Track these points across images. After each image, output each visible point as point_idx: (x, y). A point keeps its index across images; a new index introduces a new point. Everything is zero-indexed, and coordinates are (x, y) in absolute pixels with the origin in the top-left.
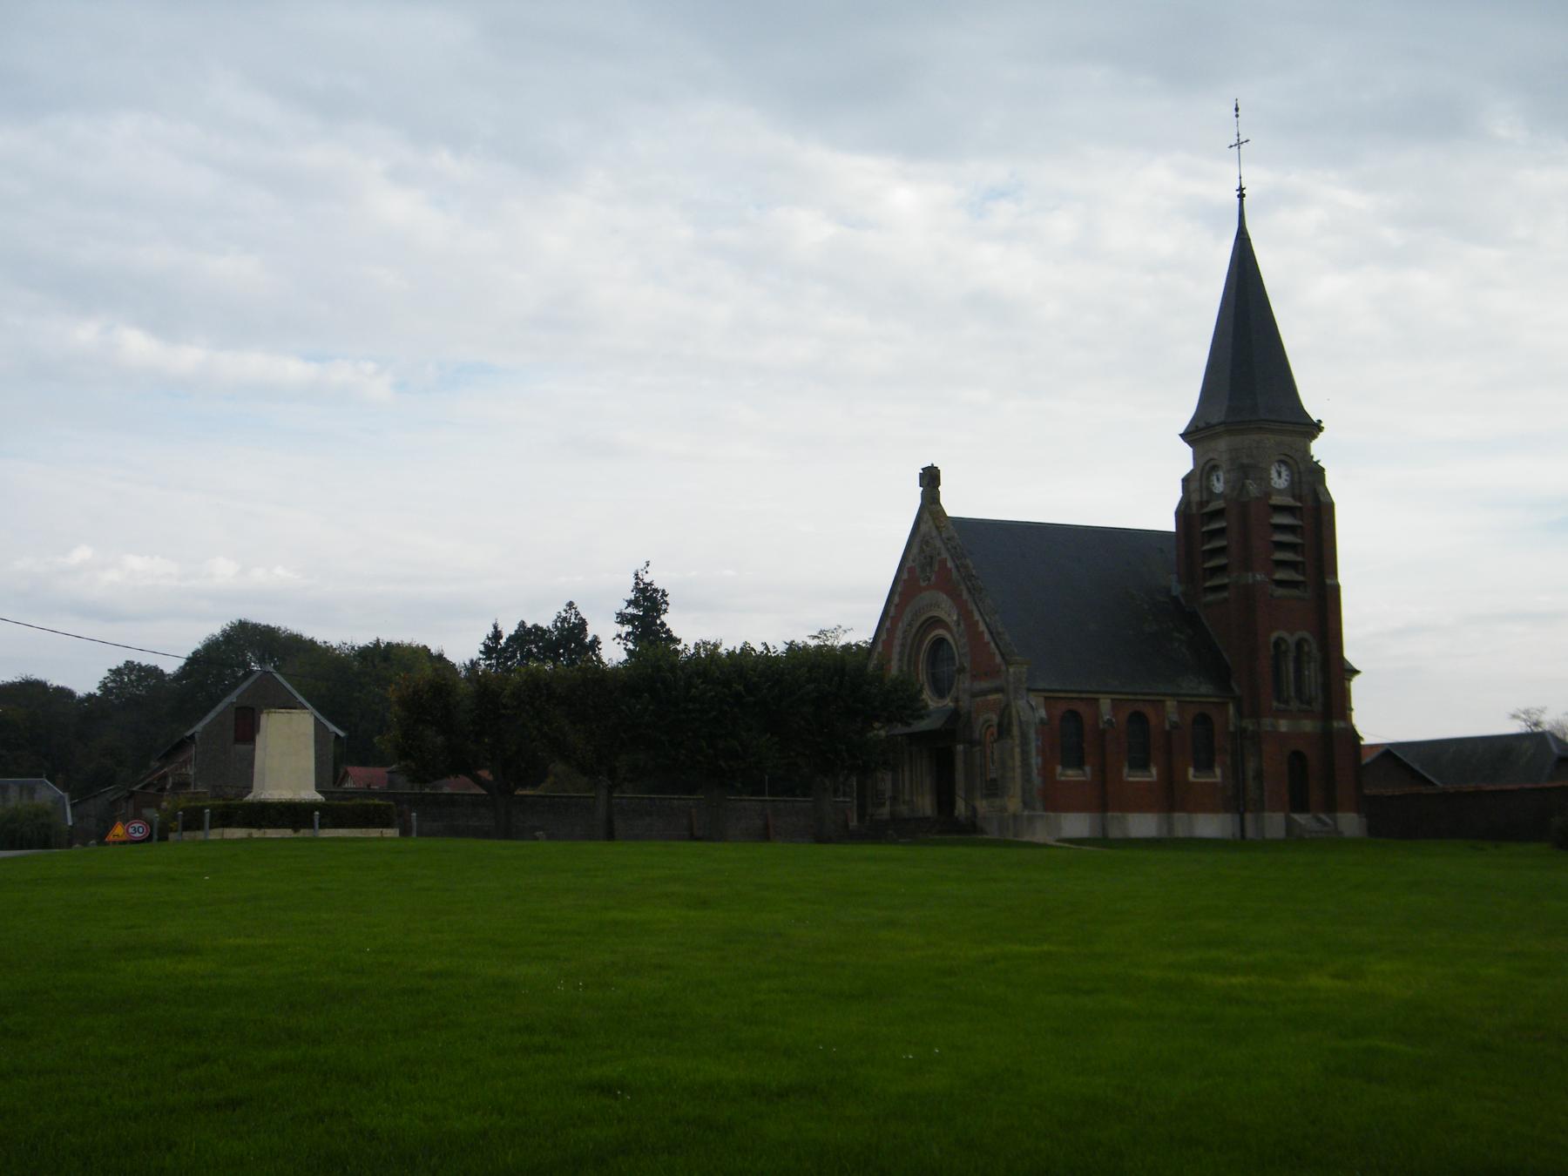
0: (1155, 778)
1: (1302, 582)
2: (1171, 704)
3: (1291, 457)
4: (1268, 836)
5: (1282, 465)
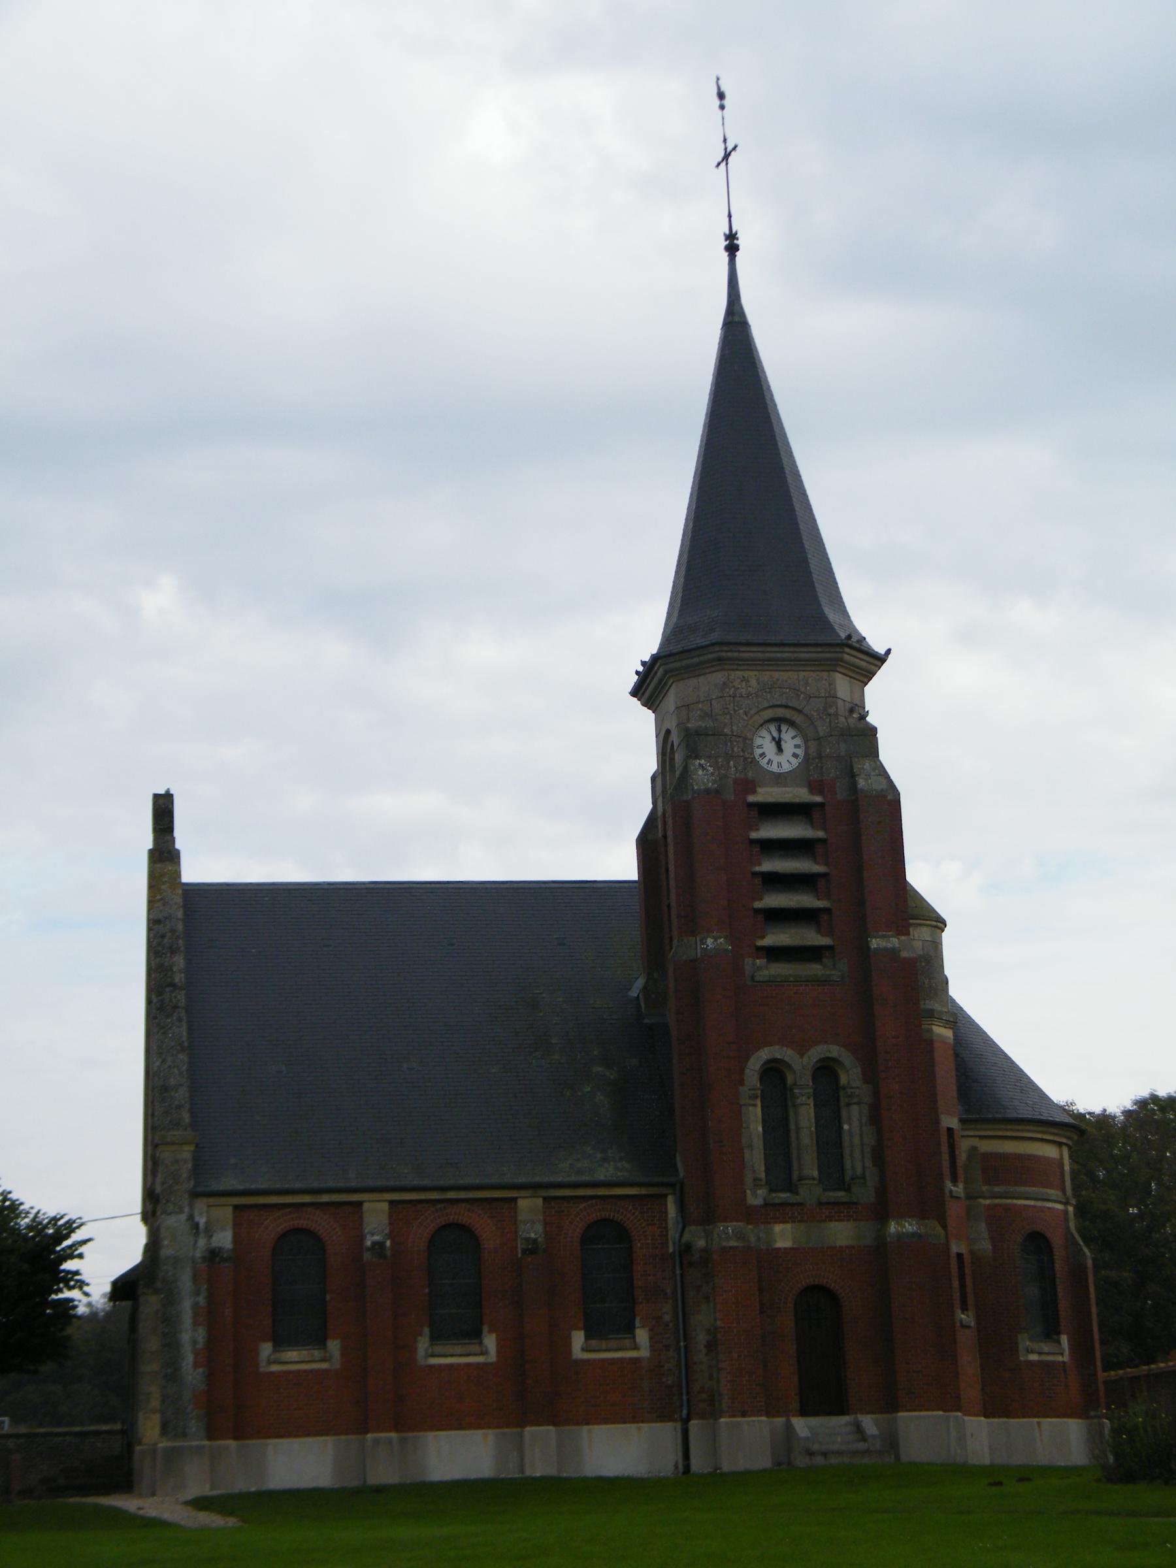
0: (492, 1357)
1: (830, 948)
2: (528, 1206)
3: (800, 711)
4: (726, 1467)
5: (784, 728)
